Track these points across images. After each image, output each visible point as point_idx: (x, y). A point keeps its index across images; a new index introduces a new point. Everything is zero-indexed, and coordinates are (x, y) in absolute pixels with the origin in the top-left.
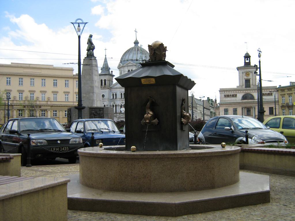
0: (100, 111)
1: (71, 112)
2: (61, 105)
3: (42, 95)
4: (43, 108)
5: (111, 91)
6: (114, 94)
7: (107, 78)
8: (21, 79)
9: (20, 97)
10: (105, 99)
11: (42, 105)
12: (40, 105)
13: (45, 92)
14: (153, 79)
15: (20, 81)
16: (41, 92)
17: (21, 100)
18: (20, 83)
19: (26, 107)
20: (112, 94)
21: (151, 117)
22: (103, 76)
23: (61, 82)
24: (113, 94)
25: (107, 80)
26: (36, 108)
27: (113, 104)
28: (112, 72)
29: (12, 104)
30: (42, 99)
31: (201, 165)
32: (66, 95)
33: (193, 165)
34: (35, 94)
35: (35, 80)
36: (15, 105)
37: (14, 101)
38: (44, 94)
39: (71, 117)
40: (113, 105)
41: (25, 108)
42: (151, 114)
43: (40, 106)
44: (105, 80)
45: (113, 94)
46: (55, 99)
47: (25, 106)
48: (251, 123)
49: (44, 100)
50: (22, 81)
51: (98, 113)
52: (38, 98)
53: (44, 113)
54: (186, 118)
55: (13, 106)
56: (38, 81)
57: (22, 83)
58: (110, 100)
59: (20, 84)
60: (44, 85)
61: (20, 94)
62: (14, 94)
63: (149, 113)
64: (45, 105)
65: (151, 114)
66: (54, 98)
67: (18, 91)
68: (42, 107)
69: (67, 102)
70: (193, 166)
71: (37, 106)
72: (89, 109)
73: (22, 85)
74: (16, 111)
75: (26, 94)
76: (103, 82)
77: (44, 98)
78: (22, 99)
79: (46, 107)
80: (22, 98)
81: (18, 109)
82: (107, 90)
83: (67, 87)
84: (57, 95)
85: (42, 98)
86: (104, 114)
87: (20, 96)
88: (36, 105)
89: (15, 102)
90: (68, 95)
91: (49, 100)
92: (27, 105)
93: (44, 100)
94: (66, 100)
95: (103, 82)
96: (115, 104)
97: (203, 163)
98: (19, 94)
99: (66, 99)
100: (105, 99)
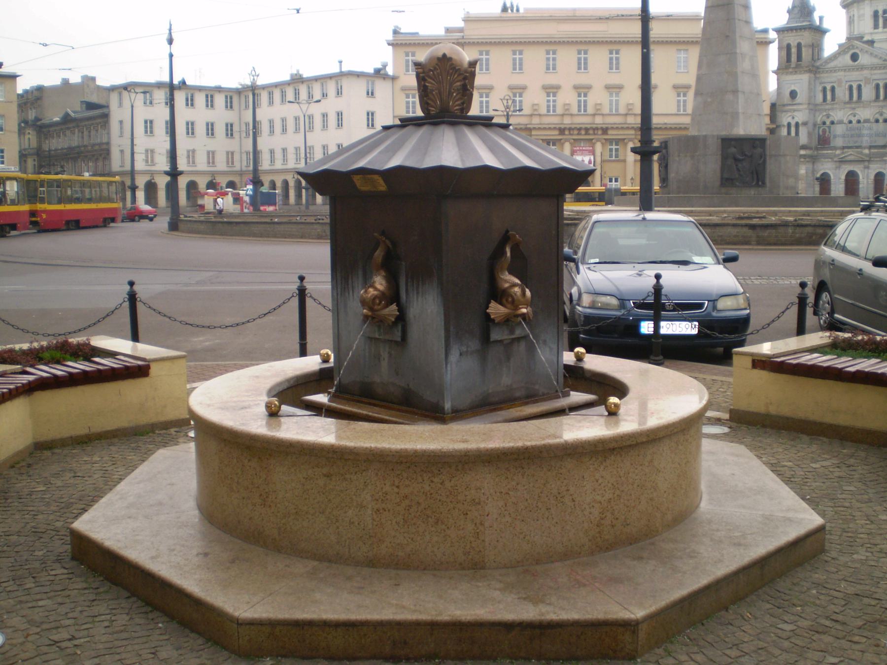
0: (754, 147)
1: (667, 152)
2: (666, 124)
3: (611, 95)
4: (612, 134)
5: (818, 78)
6: (828, 87)
7: (806, 38)
8: (553, 54)
9: (548, 106)
10: (799, 104)
11: (610, 126)
12: (604, 126)
13: (620, 87)
14: (376, 177)
15: (548, 59)
16: (608, 87)
17: (551, 113)
18: (549, 65)
19: (567, 132)
20: (820, 88)
21: (375, 298)
22: (794, 33)
23: (598, 58)
24: (851, 88)
25: (805, 46)
26: (594, 134)
27: (825, 119)
28: (821, 18)
29: (528, 126)
30: (611, 110)
31: (427, 488)
32: (679, 95)
33: (398, 487)
34: (589, 95)
35: (524, 52)
36: (534, 128)
37: (596, 117)
38: (617, 94)
39: (666, 167)
40: (789, 125)
41: (564, 134)
42: (376, 289)
43: (605, 131)
44: (799, 46)
45: (851, 88)
46: (582, 106)
47: (562, 131)
48: (88, 266)
49: (617, 110)
50: (554, 59)
51: (745, 155)
52: (536, 107)
53: (617, 150)
54: (507, 300)
55: (530, 130)
56: (534, 58)
57: (554, 65)
58: (813, 108)
59: (548, 69)
60: (551, 67)
61: (548, 96)
62: (533, 98)
63: (372, 286)
64: (620, 126)
65: (376, 289)
66: (579, 106)
67: (576, 87)
68: (610, 132)
69: (552, 115)
70: (396, 490)
71: (597, 129)
72: (720, 141)
73: (554, 69)
74: (602, 144)
75: (567, 98)
76: (794, 50)
77: (617, 105)
78: (554, 111)
79: (621, 132)
80: (554, 106)
81: (544, 138)
82: (805, 77)
83: (583, 71)
84: (491, 95)
85: (611, 104)
86: (768, 158)
87: (548, 101)
88: (594, 126)
89: (536, 121)
90: (554, 96)
91: (536, 110)
92: (568, 126)
93: (617, 110)
94: (679, 110)
95: (794, 50)
96: (831, 119)
97: (432, 482)
98: (545, 95)
99: (679, 106)
100: (799, 104)
